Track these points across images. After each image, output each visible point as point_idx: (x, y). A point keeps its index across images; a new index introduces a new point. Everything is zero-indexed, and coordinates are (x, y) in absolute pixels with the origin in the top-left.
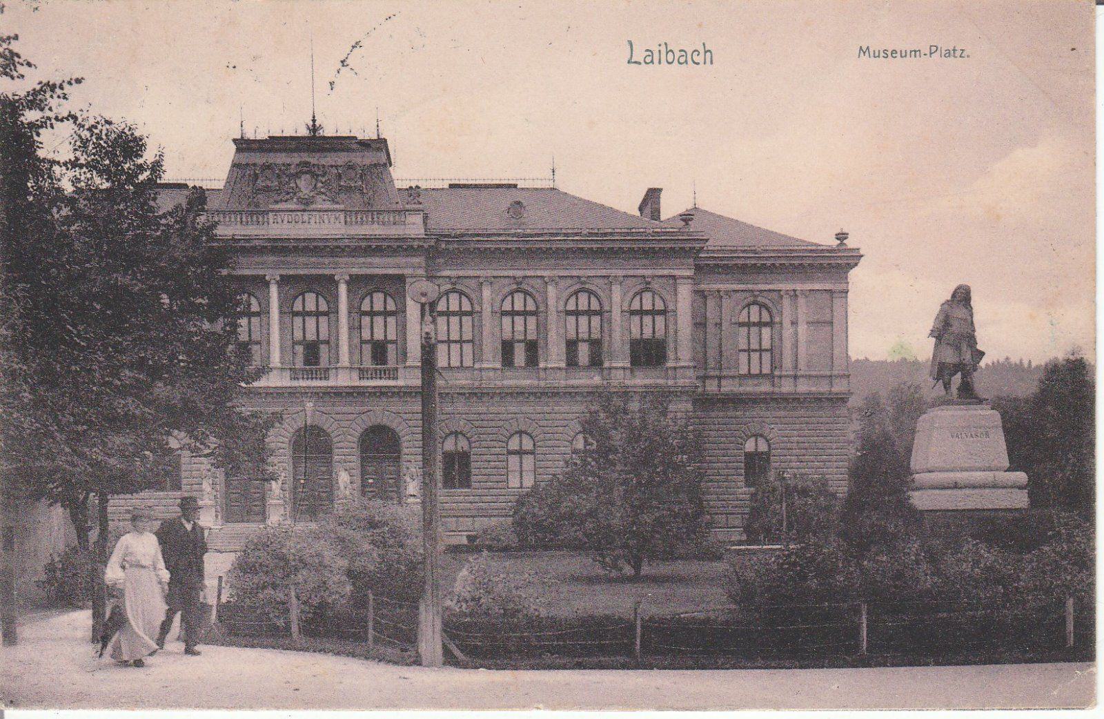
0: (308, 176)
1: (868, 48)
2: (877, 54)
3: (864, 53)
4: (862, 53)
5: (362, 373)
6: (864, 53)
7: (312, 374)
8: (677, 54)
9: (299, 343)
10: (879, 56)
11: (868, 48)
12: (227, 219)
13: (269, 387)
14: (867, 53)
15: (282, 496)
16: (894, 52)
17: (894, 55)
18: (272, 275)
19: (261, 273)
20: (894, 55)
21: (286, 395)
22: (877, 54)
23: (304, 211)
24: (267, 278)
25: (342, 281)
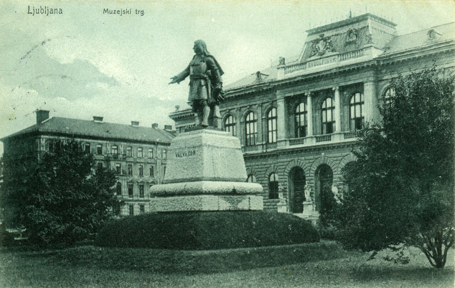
0: (322, 41)
1: (107, 9)
2: (111, 12)
3: (106, 11)
4: (105, 12)
5: (318, 139)
6: (106, 11)
7: (350, 135)
8: (58, 10)
9: (325, 123)
10: (112, 13)
11: (107, 9)
12: (349, 56)
13: (325, 145)
14: (107, 12)
15: (311, 200)
16: (118, 11)
17: (118, 13)
18: (335, 88)
19: (330, 87)
20: (118, 13)
21: (299, 151)
22: (111, 12)
23: (320, 58)
24: (333, 89)
25: (308, 96)
